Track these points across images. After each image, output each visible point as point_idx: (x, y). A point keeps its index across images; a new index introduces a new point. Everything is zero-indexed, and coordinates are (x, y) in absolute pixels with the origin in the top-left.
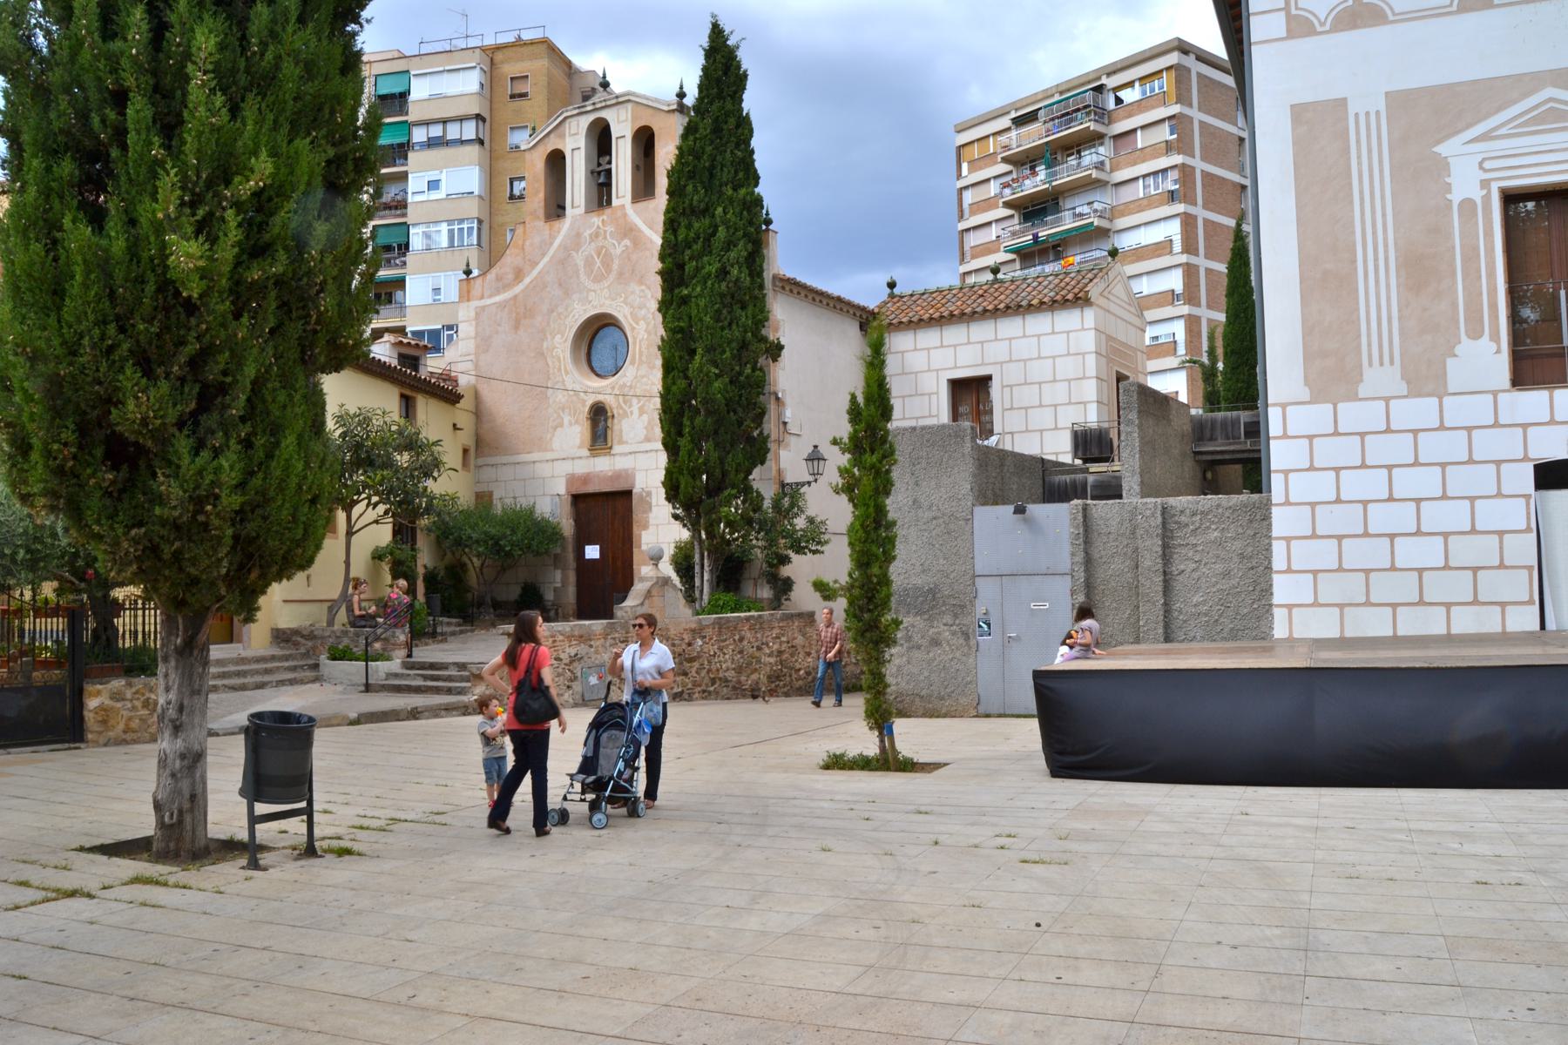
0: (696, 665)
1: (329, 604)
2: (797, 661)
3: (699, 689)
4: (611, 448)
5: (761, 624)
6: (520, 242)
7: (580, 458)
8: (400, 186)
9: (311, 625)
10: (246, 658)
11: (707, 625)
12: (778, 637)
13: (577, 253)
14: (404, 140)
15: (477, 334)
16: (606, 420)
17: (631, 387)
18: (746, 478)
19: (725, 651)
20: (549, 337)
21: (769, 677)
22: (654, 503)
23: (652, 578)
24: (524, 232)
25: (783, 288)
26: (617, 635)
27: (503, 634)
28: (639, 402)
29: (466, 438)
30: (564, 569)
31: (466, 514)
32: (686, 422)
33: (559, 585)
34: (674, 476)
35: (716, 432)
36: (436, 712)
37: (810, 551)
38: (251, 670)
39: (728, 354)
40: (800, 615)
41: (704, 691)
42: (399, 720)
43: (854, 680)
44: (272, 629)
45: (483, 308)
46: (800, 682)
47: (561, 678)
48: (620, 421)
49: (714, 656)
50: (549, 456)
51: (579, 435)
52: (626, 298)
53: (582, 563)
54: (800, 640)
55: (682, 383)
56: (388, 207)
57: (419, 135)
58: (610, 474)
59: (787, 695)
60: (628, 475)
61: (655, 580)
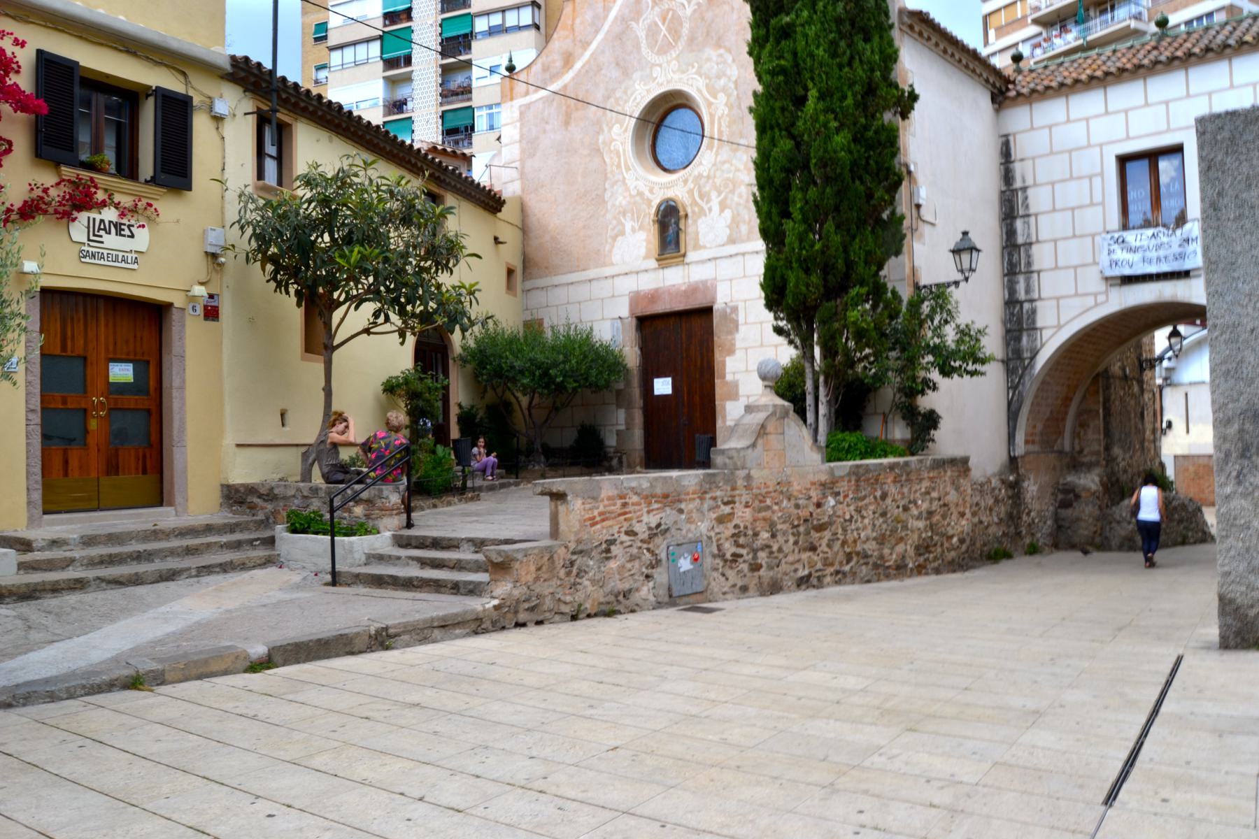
0: (827, 534)
1: (304, 449)
2: (949, 524)
3: (832, 569)
4: (684, 255)
5: (908, 474)
6: (570, 22)
7: (646, 271)
8: (466, 74)
9: (281, 480)
10: (163, 532)
11: (842, 477)
12: (928, 493)
13: (638, 23)
14: (467, 31)
15: (522, 136)
16: (677, 224)
17: (708, 177)
18: (876, 274)
19: (864, 513)
20: (605, 128)
21: (917, 548)
22: (741, 320)
23: (766, 406)
24: (574, 10)
25: (911, 27)
26: (718, 493)
27: (543, 494)
28: (719, 195)
29: (510, 254)
30: (629, 407)
31: (512, 340)
32: (796, 195)
33: (623, 427)
34: (778, 273)
35: (837, 209)
36: (424, 632)
37: (968, 372)
38: (161, 550)
39: (849, 101)
40: (953, 462)
41: (837, 572)
42: (352, 653)
43: (996, 545)
44: (222, 486)
45: (528, 106)
46: (953, 554)
47: (637, 564)
48: (695, 222)
49: (850, 520)
50: (608, 271)
51: (645, 244)
52: (700, 67)
53: (652, 404)
54: (952, 497)
55: (786, 144)
56: (455, 94)
57: (481, 25)
58: (683, 288)
59: (937, 571)
60: (708, 287)
61: (771, 409)
